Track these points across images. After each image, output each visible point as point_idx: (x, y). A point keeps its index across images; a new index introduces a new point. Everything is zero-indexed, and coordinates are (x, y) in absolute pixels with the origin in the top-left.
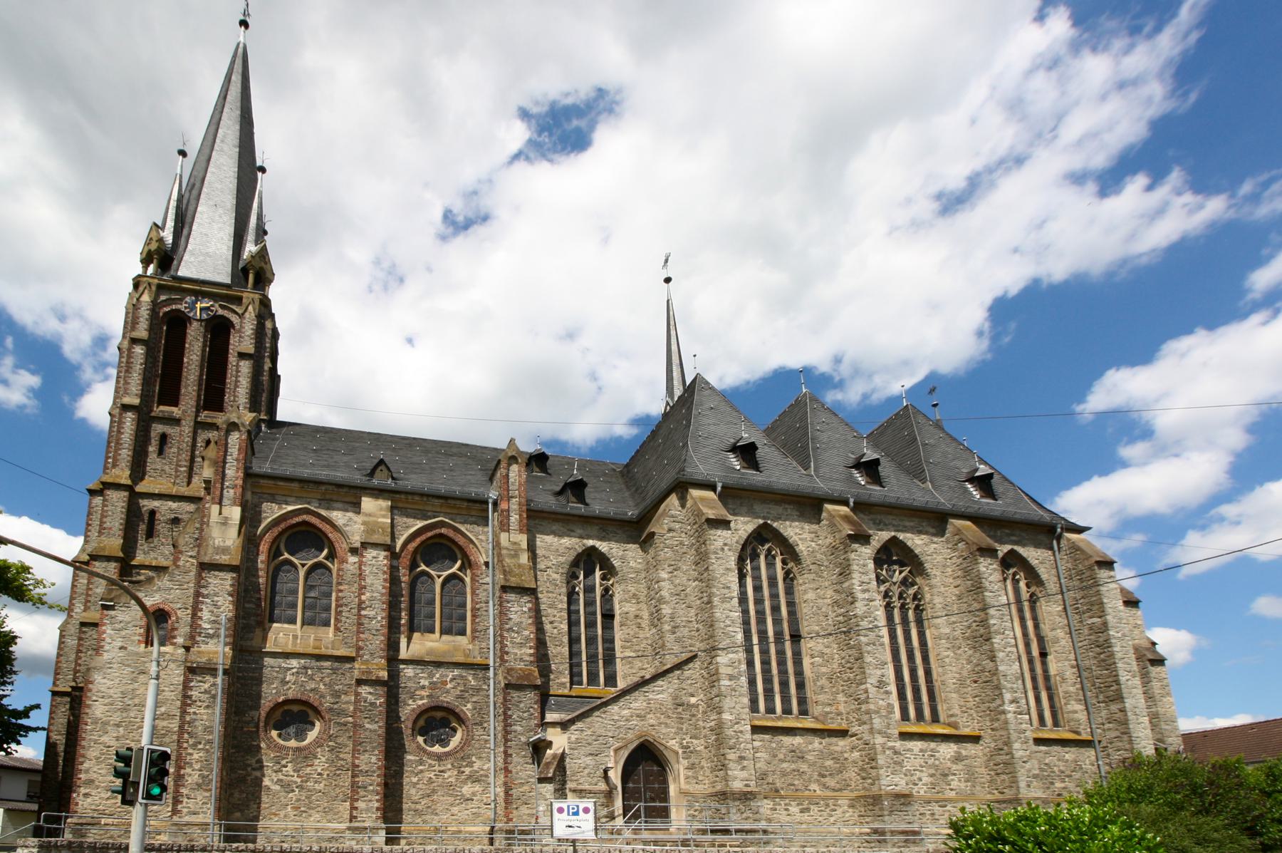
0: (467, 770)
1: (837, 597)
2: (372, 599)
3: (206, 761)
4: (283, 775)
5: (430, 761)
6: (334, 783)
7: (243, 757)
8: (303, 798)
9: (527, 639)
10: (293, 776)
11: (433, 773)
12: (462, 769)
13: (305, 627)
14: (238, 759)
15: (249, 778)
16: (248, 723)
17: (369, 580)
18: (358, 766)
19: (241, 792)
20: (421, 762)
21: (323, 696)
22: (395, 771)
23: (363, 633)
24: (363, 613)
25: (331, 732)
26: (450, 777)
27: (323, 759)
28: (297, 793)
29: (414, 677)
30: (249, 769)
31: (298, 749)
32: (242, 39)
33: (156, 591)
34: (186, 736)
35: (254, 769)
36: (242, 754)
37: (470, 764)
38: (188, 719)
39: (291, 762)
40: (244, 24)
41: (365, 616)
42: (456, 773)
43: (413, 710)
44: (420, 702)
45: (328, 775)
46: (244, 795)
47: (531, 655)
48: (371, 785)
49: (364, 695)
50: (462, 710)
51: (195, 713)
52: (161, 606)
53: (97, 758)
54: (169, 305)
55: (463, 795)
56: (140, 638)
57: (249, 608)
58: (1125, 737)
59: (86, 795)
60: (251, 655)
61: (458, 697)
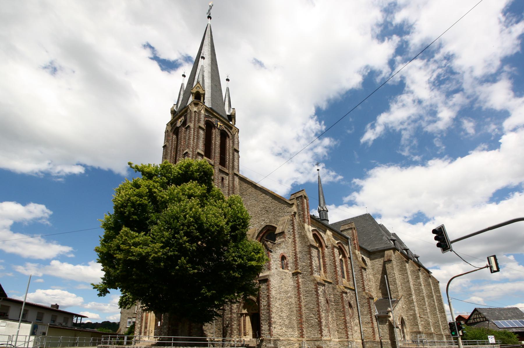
1: (414, 283)
32: (209, 23)
40: (209, 17)
53: (276, 313)
54: (208, 118)
58: (445, 321)
59: (274, 328)
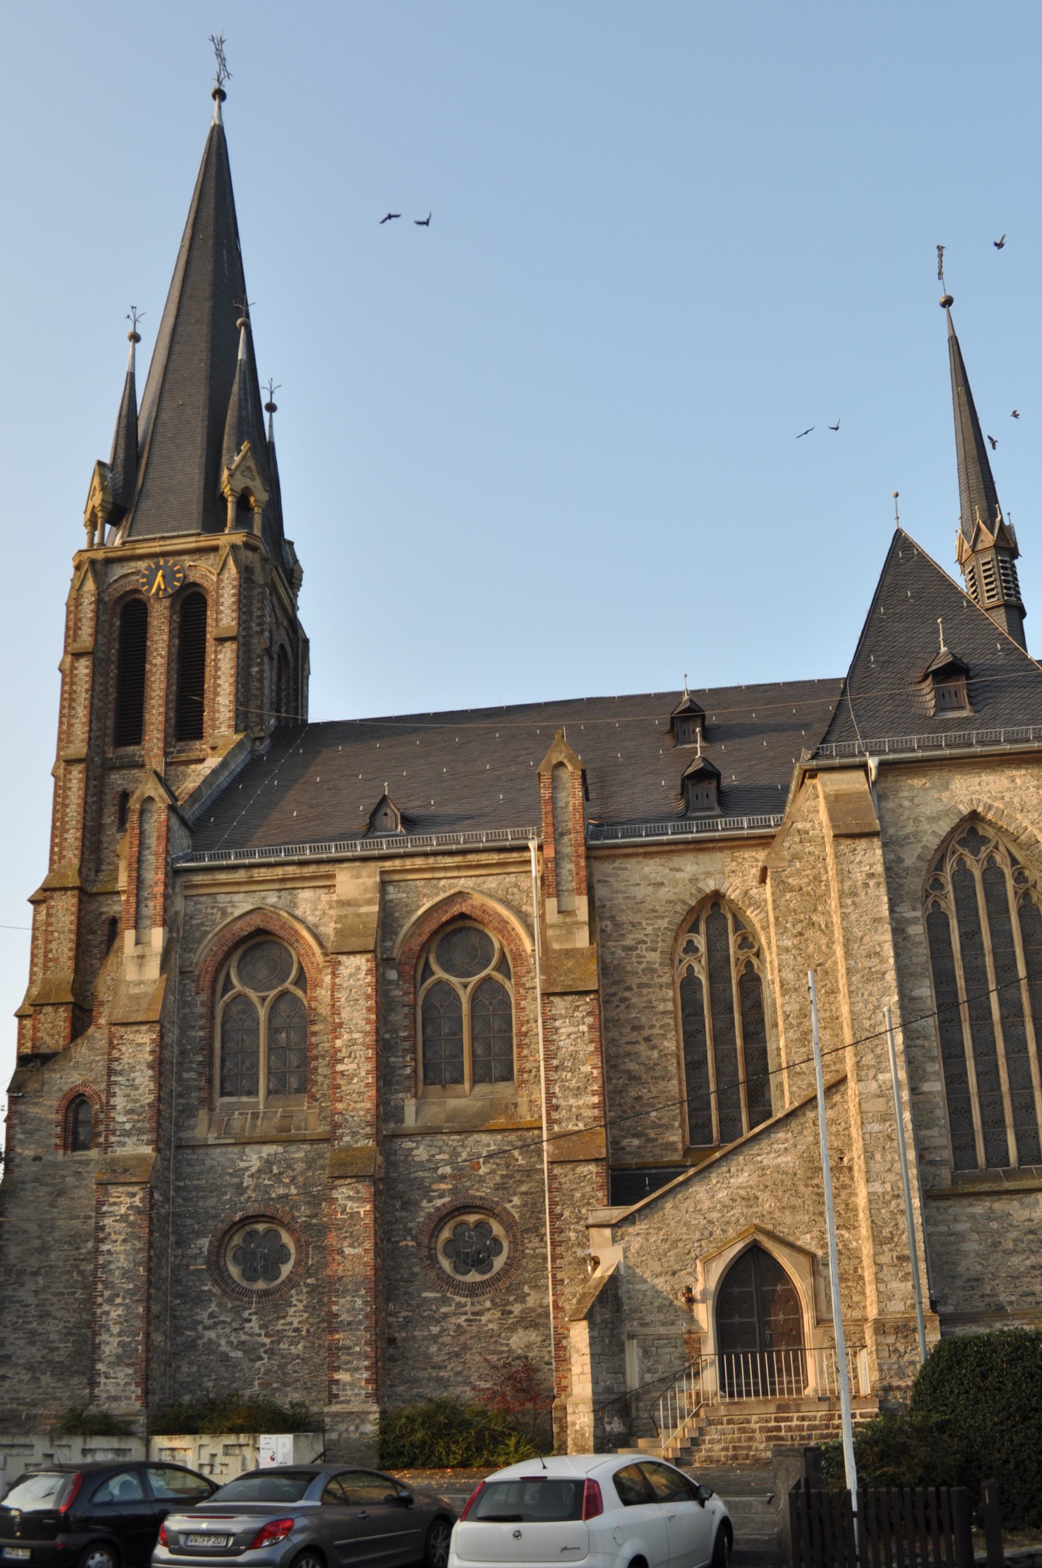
0: (517, 1309)
2: (353, 1042)
3: (126, 1321)
4: (245, 1333)
5: (458, 1299)
6: (317, 1342)
7: (191, 1310)
8: (275, 1368)
9: (588, 1077)
10: (260, 1335)
11: (464, 1318)
12: (509, 1308)
13: (271, 1097)
14: (185, 1314)
15: (200, 1342)
16: (195, 1257)
17: (345, 1014)
18: (337, 1315)
19: (191, 1363)
20: (445, 1301)
21: (295, 1207)
22: (405, 1318)
23: (341, 1101)
24: (339, 1067)
25: (310, 1263)
26: (490, 1321)
27: (300, 1306)
28: (265, 1361)
29: (429, 1161)
30: (200, 1328)
31: (266, 1293)
33: (74, 1068)
34: (100, 1286)
35: (206, 1328)
36: (189, 1306)
37: (522, 1298)
38: (101, 1262)
39: (255, 1313)
41: (342, 1073)
42: (498, 1314)
43: (429, 1216)
44: (439, 1202)
45: (308, 1331)
46: (195, 1369)
47: (594, 1106)
48: (356, 1345)
49: (341, 1202)
50: (505, 1209)
51: (109, 1252)
52: (81, 1090)
55: (510, 1351)
56: (58, 1141)
57: (189, 1079)
60: (194, 1153)
61: (497, 1188)
